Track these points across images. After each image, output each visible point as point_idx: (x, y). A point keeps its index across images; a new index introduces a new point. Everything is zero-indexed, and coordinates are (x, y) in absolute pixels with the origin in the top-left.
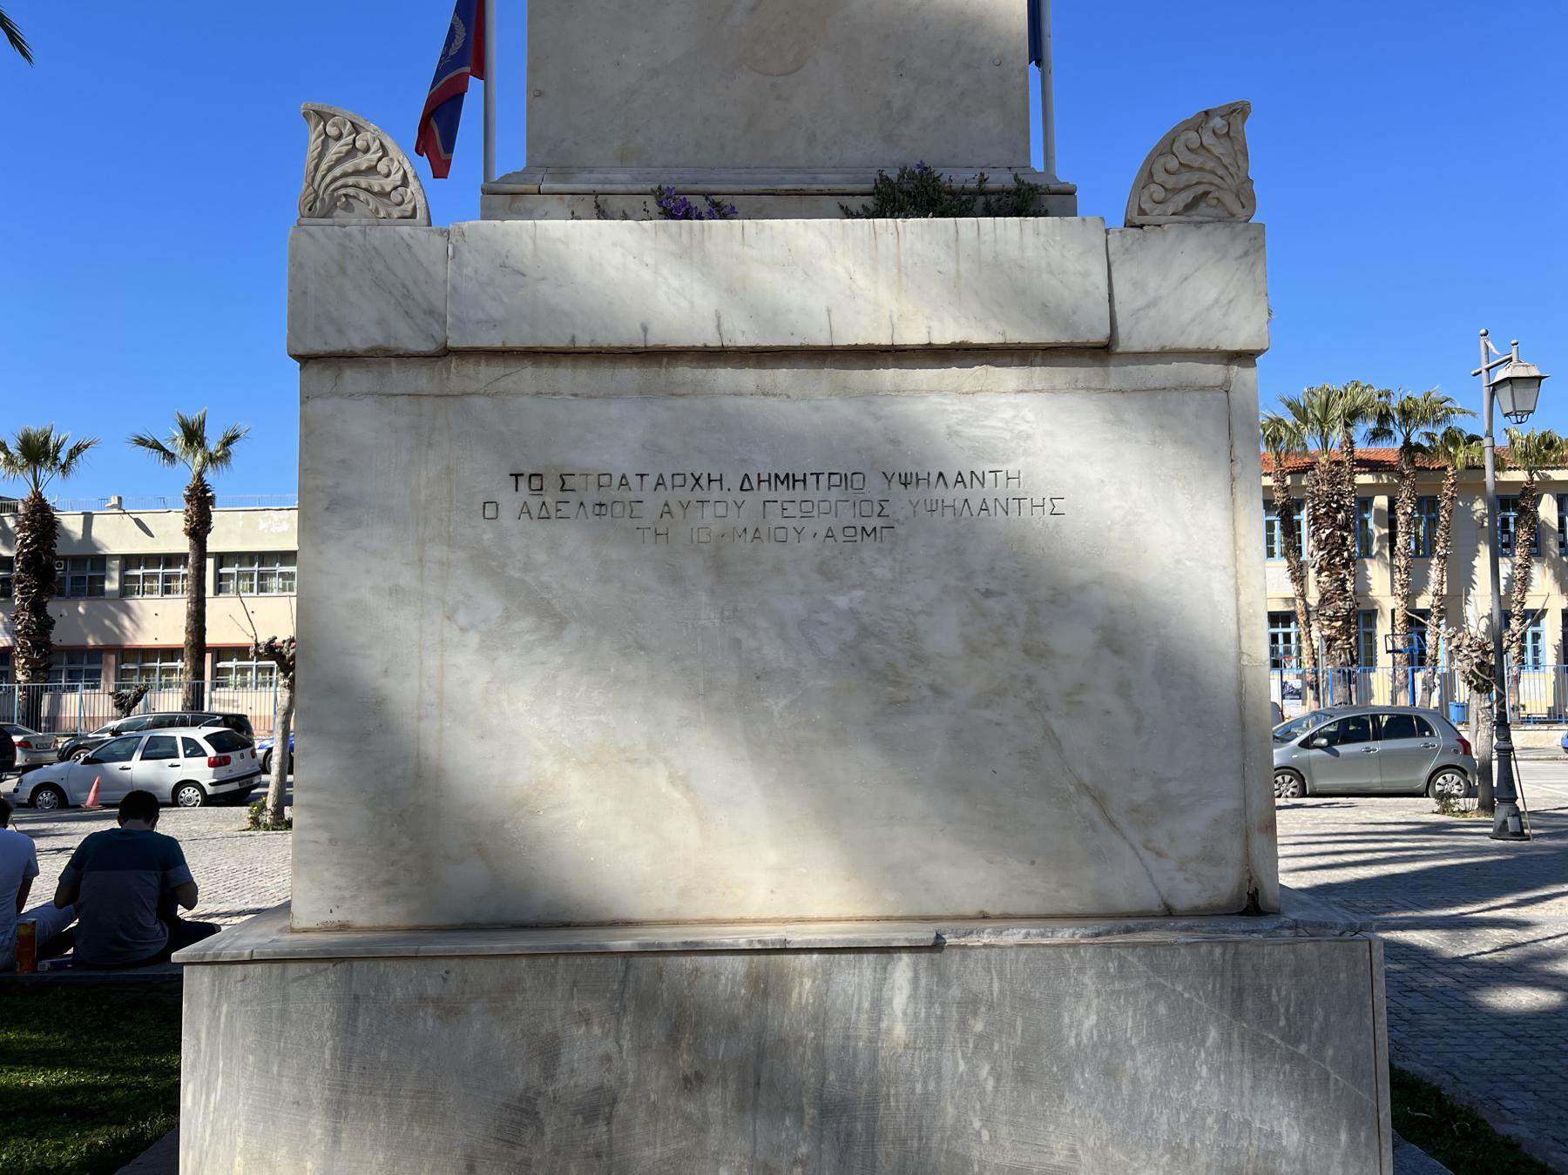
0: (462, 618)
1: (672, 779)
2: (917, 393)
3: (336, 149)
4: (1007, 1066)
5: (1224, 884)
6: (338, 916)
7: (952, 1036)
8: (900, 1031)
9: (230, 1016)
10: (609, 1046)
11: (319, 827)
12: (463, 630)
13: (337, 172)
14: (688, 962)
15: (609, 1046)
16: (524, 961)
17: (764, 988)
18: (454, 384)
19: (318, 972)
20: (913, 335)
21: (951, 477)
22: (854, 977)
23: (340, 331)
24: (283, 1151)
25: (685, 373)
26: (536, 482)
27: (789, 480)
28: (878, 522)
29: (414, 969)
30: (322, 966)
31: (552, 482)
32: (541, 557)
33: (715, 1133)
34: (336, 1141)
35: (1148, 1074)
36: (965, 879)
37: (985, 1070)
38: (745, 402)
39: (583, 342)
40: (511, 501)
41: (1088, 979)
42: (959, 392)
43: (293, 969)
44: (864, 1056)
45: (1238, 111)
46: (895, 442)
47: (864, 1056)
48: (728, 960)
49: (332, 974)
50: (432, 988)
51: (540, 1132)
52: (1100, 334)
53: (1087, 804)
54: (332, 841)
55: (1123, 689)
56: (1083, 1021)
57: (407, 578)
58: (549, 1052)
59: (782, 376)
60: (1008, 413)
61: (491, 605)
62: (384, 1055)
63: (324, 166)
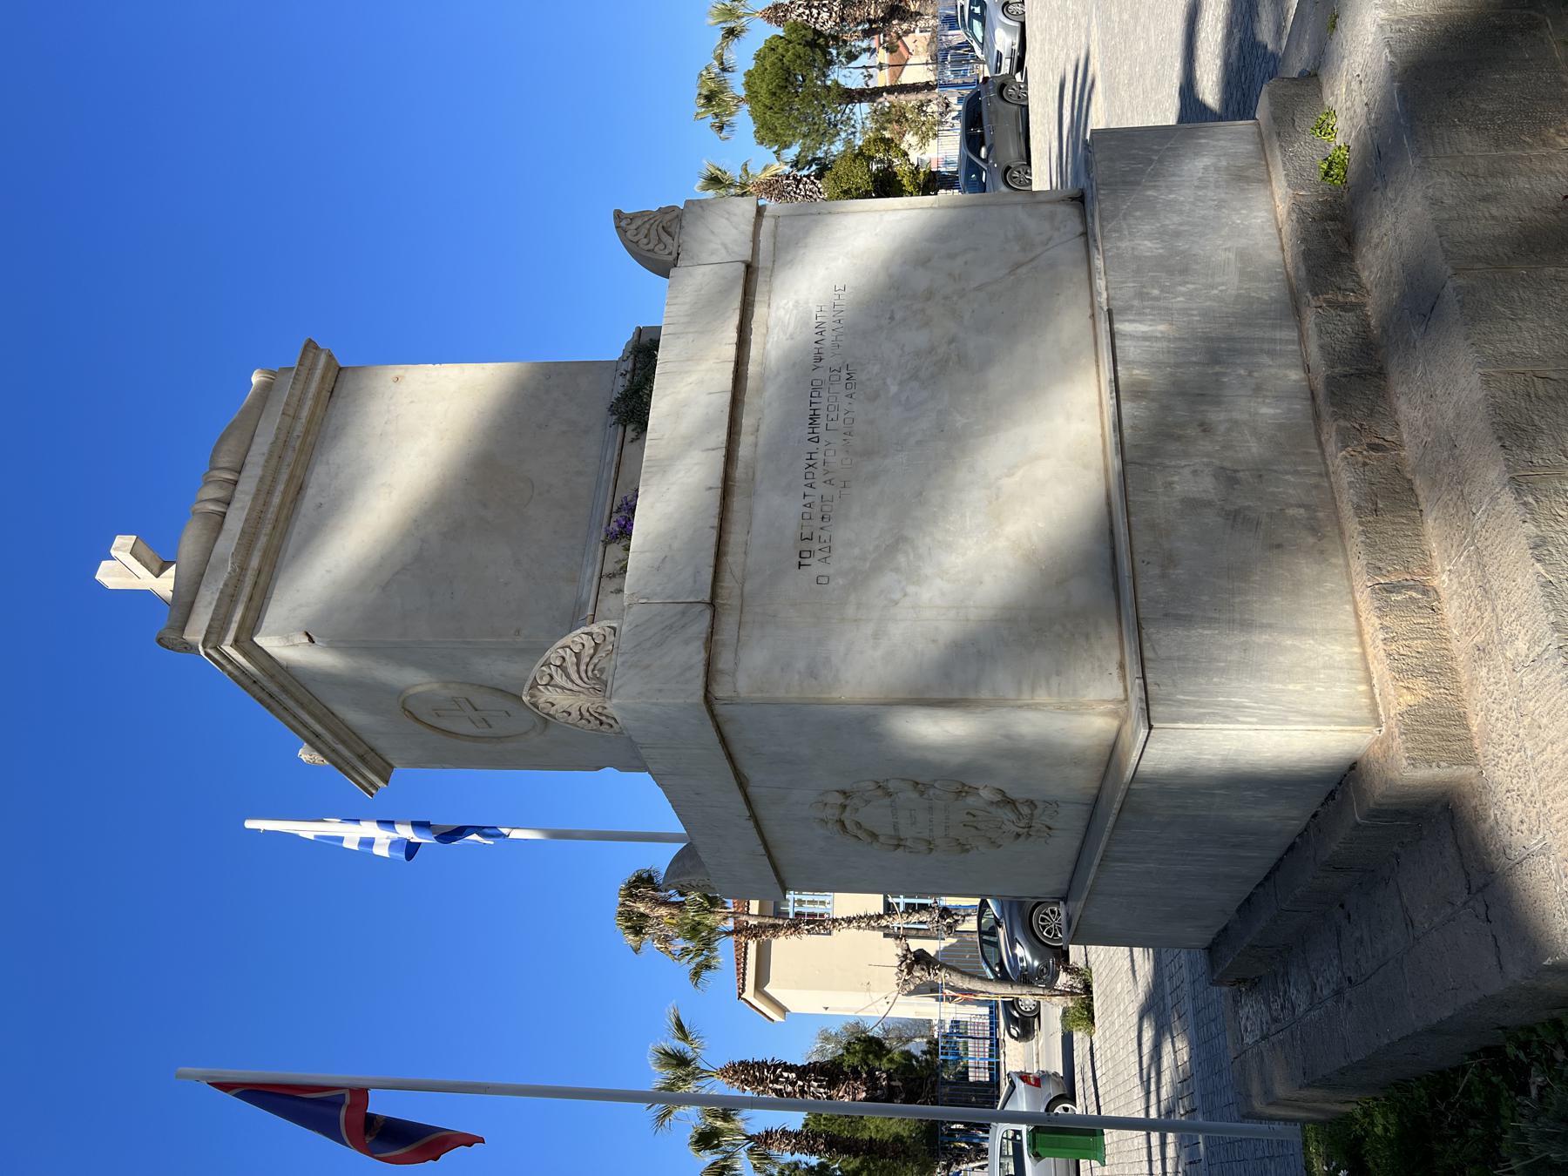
0: (897, 596)
1: (1010, 474)
2: (764, 355)
3: (559, 679)
4: (1178, 279)
5: (1068, 213)
6: (1115, 672)
7: (1161, 303)
8: (1162, 327)
9: (1183, 693)
10: (1186, 471)
11: (1047, 680)
12: (905, 595)
13: (575, 676)
14: (1127, 432)
15: (1186, 471)
16: (1133, 519)
17: (1140, 392)
18: (736, 602)
19: (1149, 639)
20: (730, 352)
21: (819, 337)
22: (1128, 349)
23: (691, 668)
24: (1281, 659)
25: (739, 472)
26: (805, 554)
27: (814, 417)
28: (844, 372)
29: (1141, 581)
30: (1144, 636)
31: (805, 545)
32: (857, 551)
33: (1236, 415)
34: (1270, 626)
35: (1176, 219)
36: (1072, 323)
37: (1183, 289)
38: (761, 441)
39: (716, 522)
40: (816, 567)
41: (1123, 245)
42: (766, 335)
43: (1148, 654)
44: (1179, 344)
45: (618, 215)
46: (794, 365)
47: (1179, 344)
48: (1123, 411)
49: (1149, 630)
50: (1155, 571)
51: (1249, 508)
52: (743, 267)
53: (1023, 270)
54: (1058, 673)
55: (952, 256)
56: (1148, 246)
57: (868, 629)
58: (1193, 505)
59: (747, 422)
60: (781, 312)
61: (888, 579)
62: (1205, 598)
63: (570, 685)
